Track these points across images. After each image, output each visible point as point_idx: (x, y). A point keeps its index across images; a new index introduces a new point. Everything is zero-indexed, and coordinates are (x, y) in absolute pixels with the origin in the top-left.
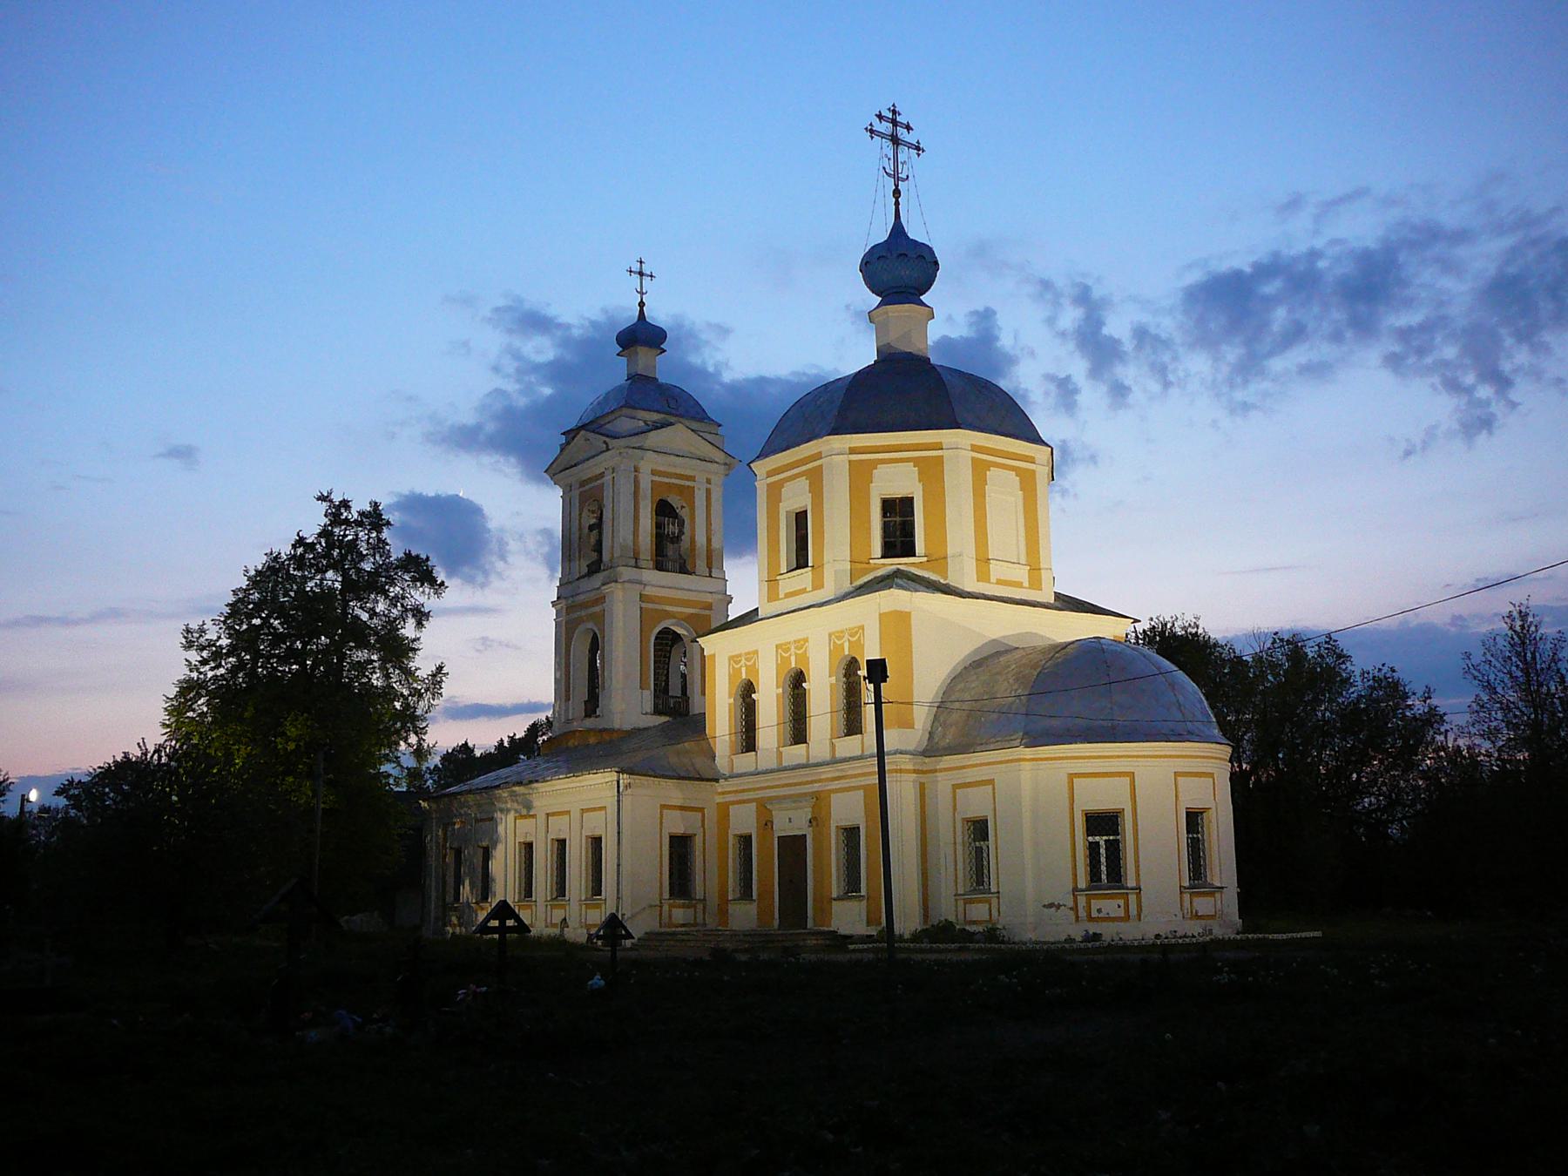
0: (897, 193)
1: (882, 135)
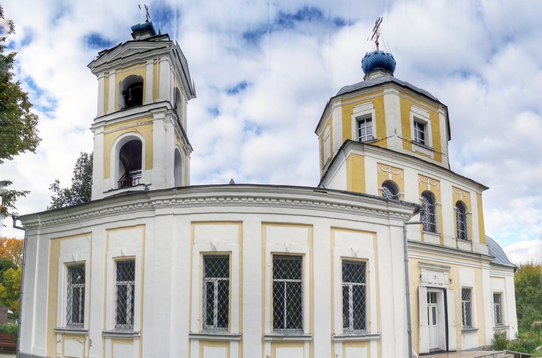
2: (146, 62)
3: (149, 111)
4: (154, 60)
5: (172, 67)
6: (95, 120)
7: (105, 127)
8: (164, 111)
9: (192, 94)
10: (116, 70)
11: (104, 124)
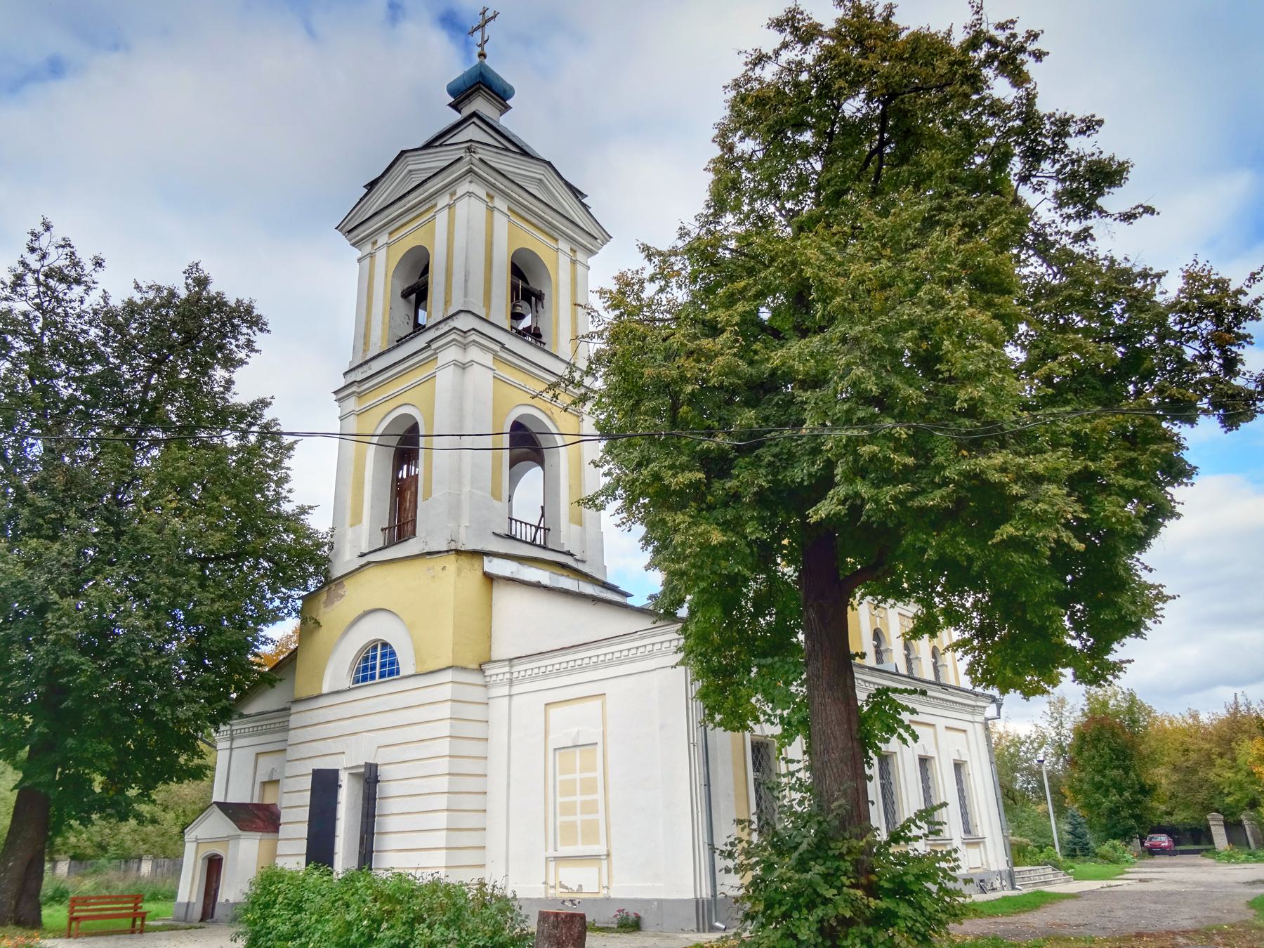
6: (345, 374)
7: (360, 395)
11: (354, 389)
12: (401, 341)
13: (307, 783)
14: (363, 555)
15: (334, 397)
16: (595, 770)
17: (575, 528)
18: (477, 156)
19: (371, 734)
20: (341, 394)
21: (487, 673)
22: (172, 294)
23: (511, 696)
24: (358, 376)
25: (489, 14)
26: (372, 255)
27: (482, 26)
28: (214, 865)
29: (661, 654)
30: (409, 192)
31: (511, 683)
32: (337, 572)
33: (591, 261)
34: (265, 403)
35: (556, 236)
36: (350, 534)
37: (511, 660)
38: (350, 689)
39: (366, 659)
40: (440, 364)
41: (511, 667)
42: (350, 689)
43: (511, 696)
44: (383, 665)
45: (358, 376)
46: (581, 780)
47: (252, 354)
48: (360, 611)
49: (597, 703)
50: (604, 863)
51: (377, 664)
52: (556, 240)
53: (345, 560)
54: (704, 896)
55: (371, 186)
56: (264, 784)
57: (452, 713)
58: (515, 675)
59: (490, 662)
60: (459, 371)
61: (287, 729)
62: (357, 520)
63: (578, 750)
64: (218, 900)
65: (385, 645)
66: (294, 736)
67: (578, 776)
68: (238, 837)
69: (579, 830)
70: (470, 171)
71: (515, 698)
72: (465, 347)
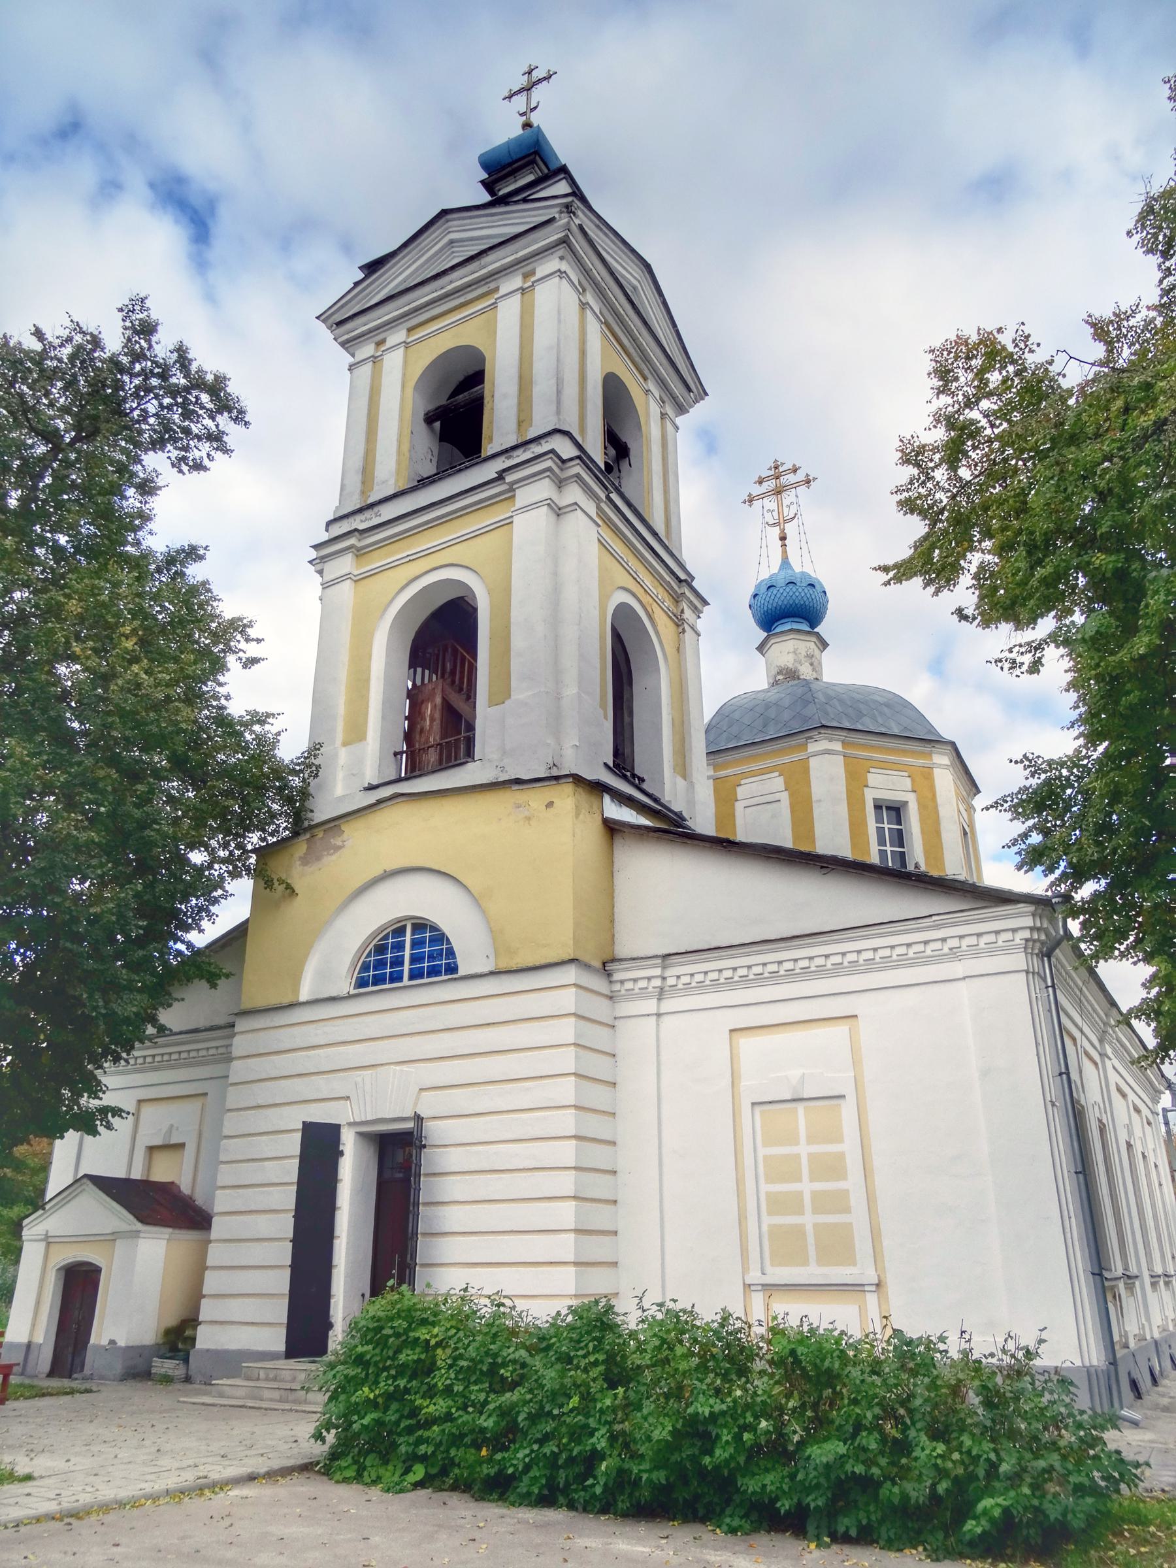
0: (783, 538)
1: (761, 496)
2: (497, 289)
3: (501, 476)
4: (526, 276)
5: (590, 298)
6: (329, 524)
7: (360, 553)
8: (549, 469)
9: (684, 388)
10: (409, 330)
11: (352, 541)
12: (424, 483)
13: (293, 1144)
14: (371, 788)
15: (313, 554)
16: (839, 1139)
17: (680, 782)
18: (577, 222)
19: (405, 1068)
20: (324, 553)
21: (617, 976)
22: (96, 342)
23: (659, 1015)
24: (359, 523)
25: (536, 75)
26: (375, 360)
27: (527, 89)
28: (79, 1286)
29: (993, 950)
30: (453, 268)
31: (661, 994)
32: (322, 810)
33: (679, 421)
34: (193, 553)
35: (646, 372)
36: (343, 756)
37: (666, 956)
38: (350, 997)
39: (380, 949)
40: (518, 506)
41: (664, 968)
42: (350, 997)
43: (659, 1015)
44: (414, 959)
45: (359, 523)
46: (811, 1156)
47: (218, 455)
48: (378, 871)
49: (842, 1029)
50: (872, 1299)
51: (409, 957)
52: (645, 379)
53: (337, 792)
54: (1095, 1363)
55: (372, 267)
56: (151, 1149)
57: (577, 1035)
58: (671, 981)
59: (613, 960)
60: (553, 517)
61: (228, 1059)
62: (356, 734)
63: (800, 1107)
64: (93, 1340)
65: (420, 926)
66: (238, 1071)
67: (803, 1150)
68: (135, 1234)
69: (811, 1240)
70: (564, 241)
71: (666, 1020)
72: (560, 484)
